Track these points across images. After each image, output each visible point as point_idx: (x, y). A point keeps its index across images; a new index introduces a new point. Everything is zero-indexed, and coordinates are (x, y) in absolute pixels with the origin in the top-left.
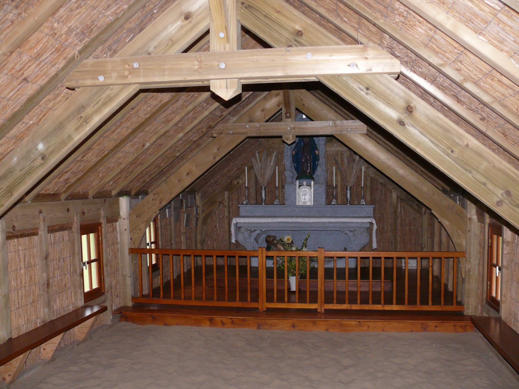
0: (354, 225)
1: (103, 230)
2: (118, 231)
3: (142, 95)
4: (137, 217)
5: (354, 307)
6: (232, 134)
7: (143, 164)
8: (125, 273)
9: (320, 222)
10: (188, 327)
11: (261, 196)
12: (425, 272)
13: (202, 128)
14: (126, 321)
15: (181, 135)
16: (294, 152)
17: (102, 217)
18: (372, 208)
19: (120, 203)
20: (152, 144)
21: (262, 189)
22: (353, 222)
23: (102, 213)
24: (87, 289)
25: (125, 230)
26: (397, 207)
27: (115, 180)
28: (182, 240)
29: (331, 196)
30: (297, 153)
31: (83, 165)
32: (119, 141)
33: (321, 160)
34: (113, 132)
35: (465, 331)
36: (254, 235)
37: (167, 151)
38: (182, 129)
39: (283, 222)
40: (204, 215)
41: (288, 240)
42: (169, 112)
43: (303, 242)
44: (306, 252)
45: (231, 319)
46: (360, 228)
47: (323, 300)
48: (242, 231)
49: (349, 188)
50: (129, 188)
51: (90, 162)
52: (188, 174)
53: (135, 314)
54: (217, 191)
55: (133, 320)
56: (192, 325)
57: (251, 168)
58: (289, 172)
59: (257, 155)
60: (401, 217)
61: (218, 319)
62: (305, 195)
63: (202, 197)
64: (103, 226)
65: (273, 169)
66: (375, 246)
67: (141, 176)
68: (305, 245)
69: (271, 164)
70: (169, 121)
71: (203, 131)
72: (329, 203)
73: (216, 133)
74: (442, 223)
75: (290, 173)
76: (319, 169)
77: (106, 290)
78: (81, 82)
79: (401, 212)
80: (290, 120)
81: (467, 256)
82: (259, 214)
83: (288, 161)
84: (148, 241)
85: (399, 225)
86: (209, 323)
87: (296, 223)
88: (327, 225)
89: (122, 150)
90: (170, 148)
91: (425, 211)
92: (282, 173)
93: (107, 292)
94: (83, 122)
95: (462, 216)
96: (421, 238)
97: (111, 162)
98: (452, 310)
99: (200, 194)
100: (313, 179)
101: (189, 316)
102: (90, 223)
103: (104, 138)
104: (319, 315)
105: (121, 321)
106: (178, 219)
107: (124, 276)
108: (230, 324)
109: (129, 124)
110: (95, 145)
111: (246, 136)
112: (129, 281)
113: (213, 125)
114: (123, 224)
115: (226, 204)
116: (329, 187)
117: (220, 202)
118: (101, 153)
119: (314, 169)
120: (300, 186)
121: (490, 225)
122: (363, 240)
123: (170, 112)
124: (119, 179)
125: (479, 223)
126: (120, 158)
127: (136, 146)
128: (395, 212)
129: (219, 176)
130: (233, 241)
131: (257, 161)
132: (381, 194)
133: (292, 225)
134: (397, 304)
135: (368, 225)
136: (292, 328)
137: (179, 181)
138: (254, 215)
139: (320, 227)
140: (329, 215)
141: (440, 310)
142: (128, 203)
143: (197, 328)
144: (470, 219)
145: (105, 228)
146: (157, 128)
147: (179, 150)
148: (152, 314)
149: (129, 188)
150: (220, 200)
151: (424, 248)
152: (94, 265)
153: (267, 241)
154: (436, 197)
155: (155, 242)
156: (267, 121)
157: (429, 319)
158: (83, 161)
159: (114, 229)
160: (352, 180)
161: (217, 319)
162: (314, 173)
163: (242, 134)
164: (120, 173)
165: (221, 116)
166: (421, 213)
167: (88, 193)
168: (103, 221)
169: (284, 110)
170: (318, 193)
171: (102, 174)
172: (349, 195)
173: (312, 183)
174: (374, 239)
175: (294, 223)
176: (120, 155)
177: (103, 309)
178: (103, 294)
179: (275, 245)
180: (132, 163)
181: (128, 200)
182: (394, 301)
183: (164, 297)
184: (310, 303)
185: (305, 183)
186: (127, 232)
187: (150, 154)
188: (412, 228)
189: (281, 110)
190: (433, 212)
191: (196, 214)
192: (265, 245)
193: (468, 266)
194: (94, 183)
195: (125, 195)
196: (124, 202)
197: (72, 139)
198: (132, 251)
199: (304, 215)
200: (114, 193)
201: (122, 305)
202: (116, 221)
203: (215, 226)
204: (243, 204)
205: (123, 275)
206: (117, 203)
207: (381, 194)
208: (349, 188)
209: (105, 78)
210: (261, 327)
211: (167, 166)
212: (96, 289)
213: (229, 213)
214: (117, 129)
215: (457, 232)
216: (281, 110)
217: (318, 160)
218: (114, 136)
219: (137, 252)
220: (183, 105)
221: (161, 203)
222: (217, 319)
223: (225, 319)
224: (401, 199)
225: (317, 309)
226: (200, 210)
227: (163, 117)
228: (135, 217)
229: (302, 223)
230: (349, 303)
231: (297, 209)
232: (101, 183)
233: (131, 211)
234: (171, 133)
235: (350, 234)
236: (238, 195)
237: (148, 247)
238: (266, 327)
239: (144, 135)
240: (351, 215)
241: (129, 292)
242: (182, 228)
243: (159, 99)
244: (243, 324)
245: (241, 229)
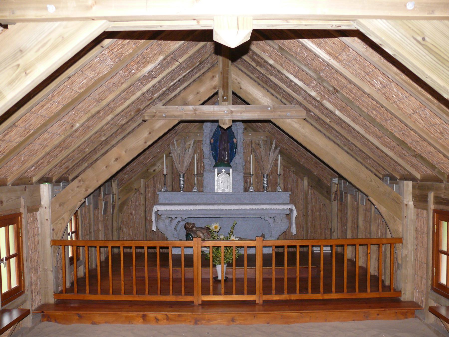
0: (274, 212)
1: (23, 220)
2: (39, 222)
3: (107, 42)
4: (60, 205)
5: (293, 297)
6: (166, 117)
7: (68, 148)
8: (46, 268)
9: (242, 209)
10: (119, 325)
11: (180, 183)
12: (340, 257)
13: (130, 111)
14: (48, 320)
15: (109, 118)
16: (212, 141)
17: (23, 206)
18: (289, 195)
19: (42, 190)
20: (82, 126)
21: (180, 177)
22: (274, 209)
23: (22, 201)
24: (5, 289)
25: (47, 220)
26: (308, 193)
27: (38, 165)
28: (100, 228)
30: (215, 141)
31: (3, 145)
32: (47, 119)
33: (239, 148)
34: (43, 106)
35: (406, 318)
36: (175, 222)
37: (94, 135)
38: (113, 110)
39: (204, 209)
40: (120, 203)
41: (216, 228)
42: (104, 88)
43: (230, 229)
44: (234, 241)
45: (166, 315)
46: (280, 214)
47: (262, 291)
48: (163, 218)
49: (265, 176)
50: (51, 174)
51: (12, 142)
52: (117, 159)
53: (58, 313)
54: (133, 179)
55: (56, 320)
56: (123, 322)
57: (169, 155)
58: (207, 160)
59: (175, 143)
60: (312, 203)
61: (151, 315)
62: (223, 182)
63: (118, 184)
64: (23, 216)
65: (191, 157)
66: (294, 231)
67: (64, 161)
68: (232, 233)
69: (190, 152)
70: (102, 100)
71: (130, 115)
72: (246, 190)
73: (147, 116)
74: (379, 209)
75: (209, 161)
76: (237, 156)
77: (26, 288)
78: (19, 14)
79: (311, 198)
80: (226, 103)
81: (404, 242)
82: (177, 202)
83: (207, 150)
84: (69, 231)
85: (310, 211)
86: (141, 320)
87: (218, 210)
88: (248, 212)
89: (49, 130)
90: (97, 132)
91: (362, 197)
92: (200, 160)
93: (28, 290)
94: (20, 73)
95: (398, 202)
96: (330, 223)
97: (36, 145)
98: (390, 296)
99: (116, 181)
100: (231, 166)
101: (120, 313)
102: (9, 213)
103: (32, 113)
104: (257, 307)
105: (43, 321)
106: (96, 207)
107: (45, 270)
108: (165, 321)
109: (61, 98)
110: (19, 122)
111: (180, 119)
112: (51, 276)
113: (142, 107)
114: (44, 213)
115: (142, 191)
116: (247, 175)
117: (136, 189)
118: (26, 132)
119: (231, 157)
120: (218, 174)
121: (435, 211)
122: (282, 226)
123: (105, 88)
124: (41, 164)
125: (416, 209)
126: (46, 140)
127: (64, 127)
128: (306, 197)
129: (135, 164)
130: (154, 229)
132: (293, 181)
133: (213, 212)
134: (336, 292)
135: (288, 212)
136: (231, 322)
137: (106, 167)
138: (173, 202)
139: (241, 214)
140: (247, 202)
141: (378, 296)
142: (50, 190)
143: (127, 326)
144: (406, 205)
145: (25, 218)
146: (89, 106)
147: (105, 135)
148: (77, 312)
149: (51, 174)
150: (136, 187)
151: (334, 232)
152: (13, 261)
153: (186, 228)
154: (373, 183)
155: (76, 232)
156: (203, 104)
157: (370, 307)
158: (4, 140)
159: (35, 219)
160: (268, 168)
161: (149, 315)
162: (231, 161)
163: (175, 117)
164: (44, 157)
165: (151, 99)
166: (330, 200)
167: (7, 179)
168: (23, 210)
169: (221, 92)
170: (236, 181)
171: (24, 157)
173: (231, 170)
174: (294, 225)
175: (215, 210)
176: (46, 136)
177: (25, 314)
178: (23, 292)
179: (195, 233)
180: (57, 146)
181: (50, 187)
182: (334, 289)
183: (90, 293)
184: (248, 294)
185: (223, 171)
186: (49, 222)
187: (77, 137)
188: (322, 213)
189: (217, 93)
190: (371, 198)
191: (113, 201)
192: (184, 232)
193: (405, 252)
194: (14, 168)
195: (46, 182)
196: (45, 190)
197: (4, 97)
198: (54, 243)
200: (35, 179)
201: (43, 302)
202: (37, 210)
203: (132, 214)
204: (161, 191)
205: (44, 269)
206: (38, 191)
207: (293, 181)
208: (265, 176)
209: (57, 8)
210: (198, 322)
211: (92, 151)
212: (15, 288)
213: (145, 200)
214: (47, 103)
215: (394, 218)
216: (217, 93)
217: (236, 148)
218: (43, 112)
219: (59, 243)
220: (119, 81)
221: (86, 190)
222: (149, 315)
223: (160, 315)
224: (311, 186)
225: (255, 301)
226: (116, 197)
227: (97, 93)
228: (58, 206)
229: (223, 210)
230: (288, 293)
231: (215, 197)
232: (23, 167)
233: (53, 199)
234: (101, 114)
235: (271, 221)
236: (154, 183)
237: (69, 238)
238: (204, 322)
239: (74, 114)
240: (268, 202)
241: (51, 288)
242: (99, 215)
243: (98, 71)
244: (179, 319)
245: (162, 216)
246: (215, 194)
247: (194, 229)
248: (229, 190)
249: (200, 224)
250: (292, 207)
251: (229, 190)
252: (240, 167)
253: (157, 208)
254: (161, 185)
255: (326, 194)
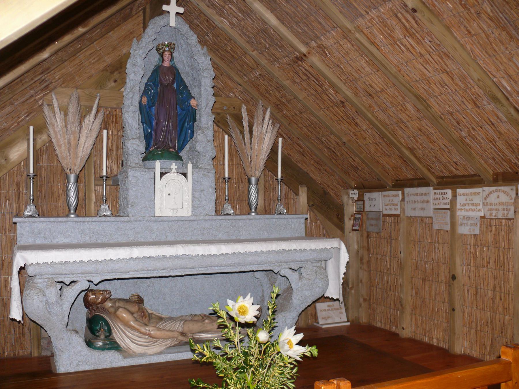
0: (298, 256)
11: (67, 196)
16: (145, 100)
19: (72, 369)
29: (231, 195)
30: (151, 103)
62: (173, 192)
72: (218, 212)
75: (135, 146)
82: (66, 241)
83: (132, 119)
120: (162, 174)
130: (16, 314)
131: (54, 113)
138: (55, 242)
140: (224, 238)
153: (87, 303)
162: (181, 148)
172: (72, 194)
199: (170, 238)
208: (253, 180)
235: (293, 277)
240: (265, 236)
246: (155, 221)
247: (109, 304)
248: (187, 211)
249: (119, 291)
250: (340, 245)
251: (187, 211)
252: (206, 162)
253: (24, 258)
254: (10, 205)
255: (336, 220)
